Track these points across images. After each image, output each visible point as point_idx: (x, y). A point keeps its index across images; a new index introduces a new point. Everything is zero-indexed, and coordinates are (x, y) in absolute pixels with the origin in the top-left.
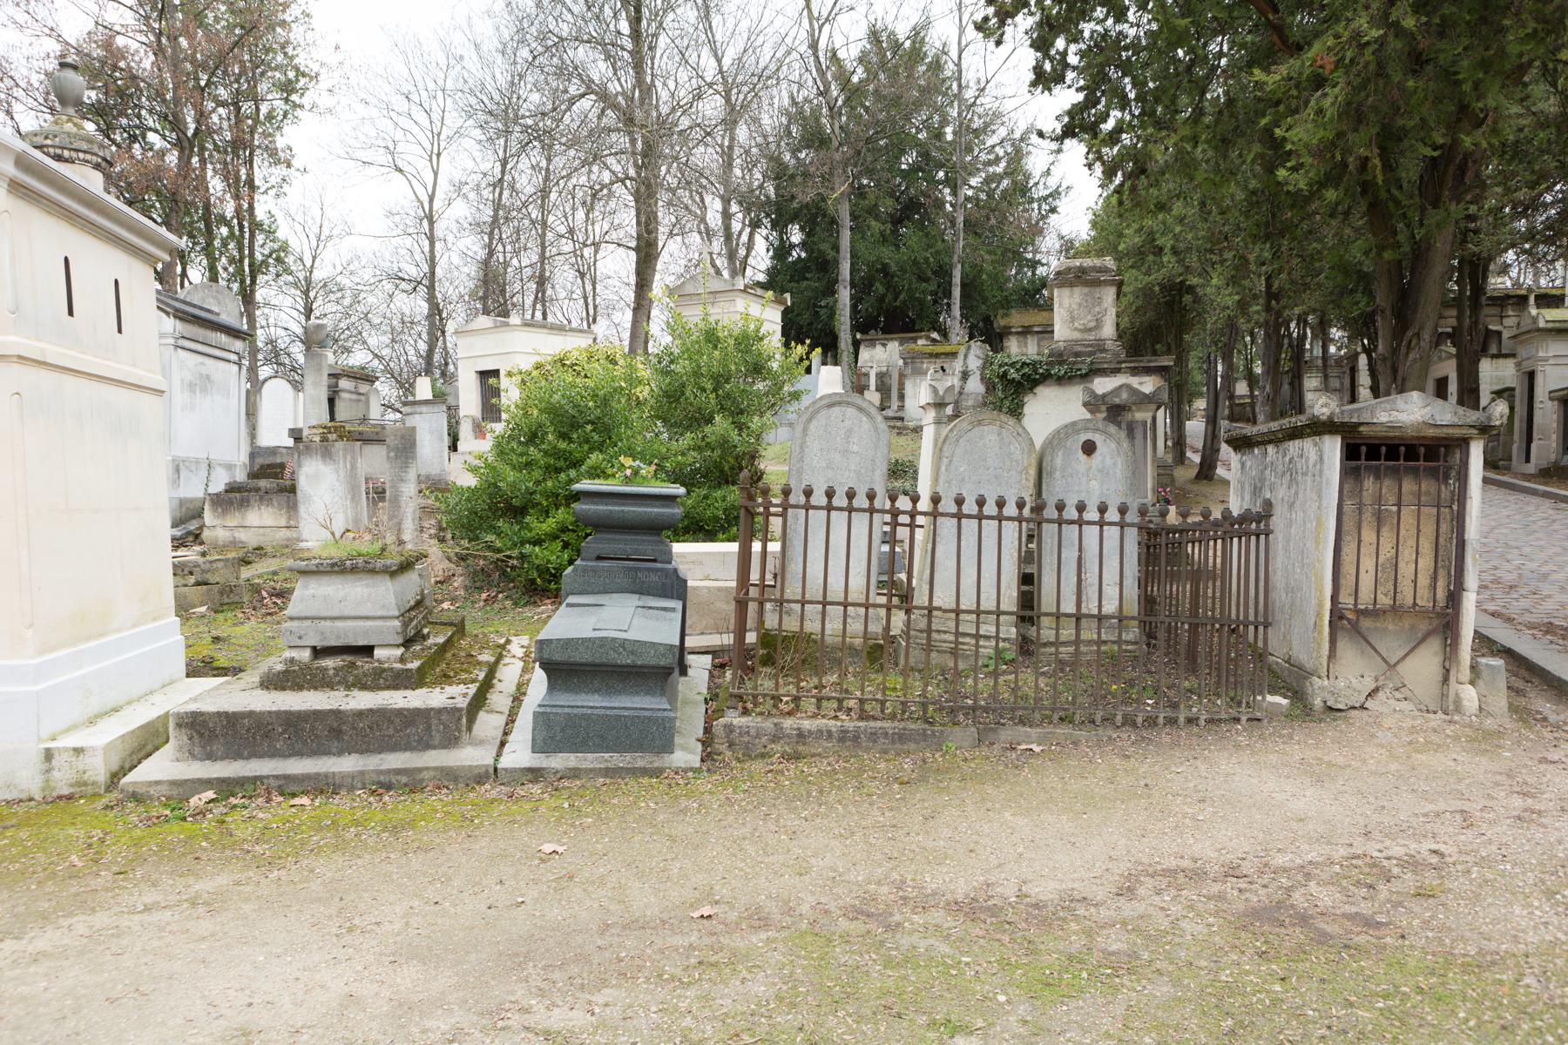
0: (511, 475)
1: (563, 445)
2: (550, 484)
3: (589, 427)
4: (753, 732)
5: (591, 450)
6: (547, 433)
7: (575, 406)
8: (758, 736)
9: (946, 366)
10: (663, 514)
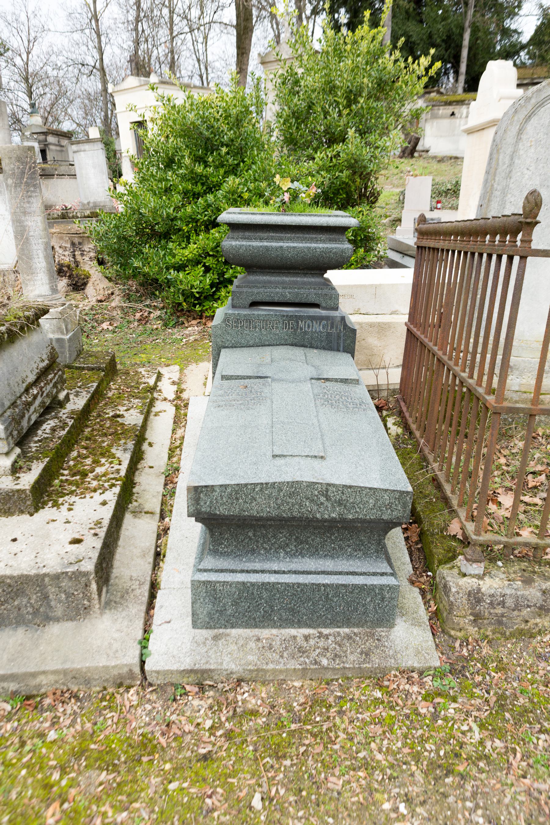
0: (152, 202)
1: (199, 169)
2: (189, 209)
3: (224, 150)
4: (510, 602)
5: (227, 174)
6: (183, 157)
7: (208, 128)
8: (517, 607)
9: (456, 111)
10: (330, 251)
